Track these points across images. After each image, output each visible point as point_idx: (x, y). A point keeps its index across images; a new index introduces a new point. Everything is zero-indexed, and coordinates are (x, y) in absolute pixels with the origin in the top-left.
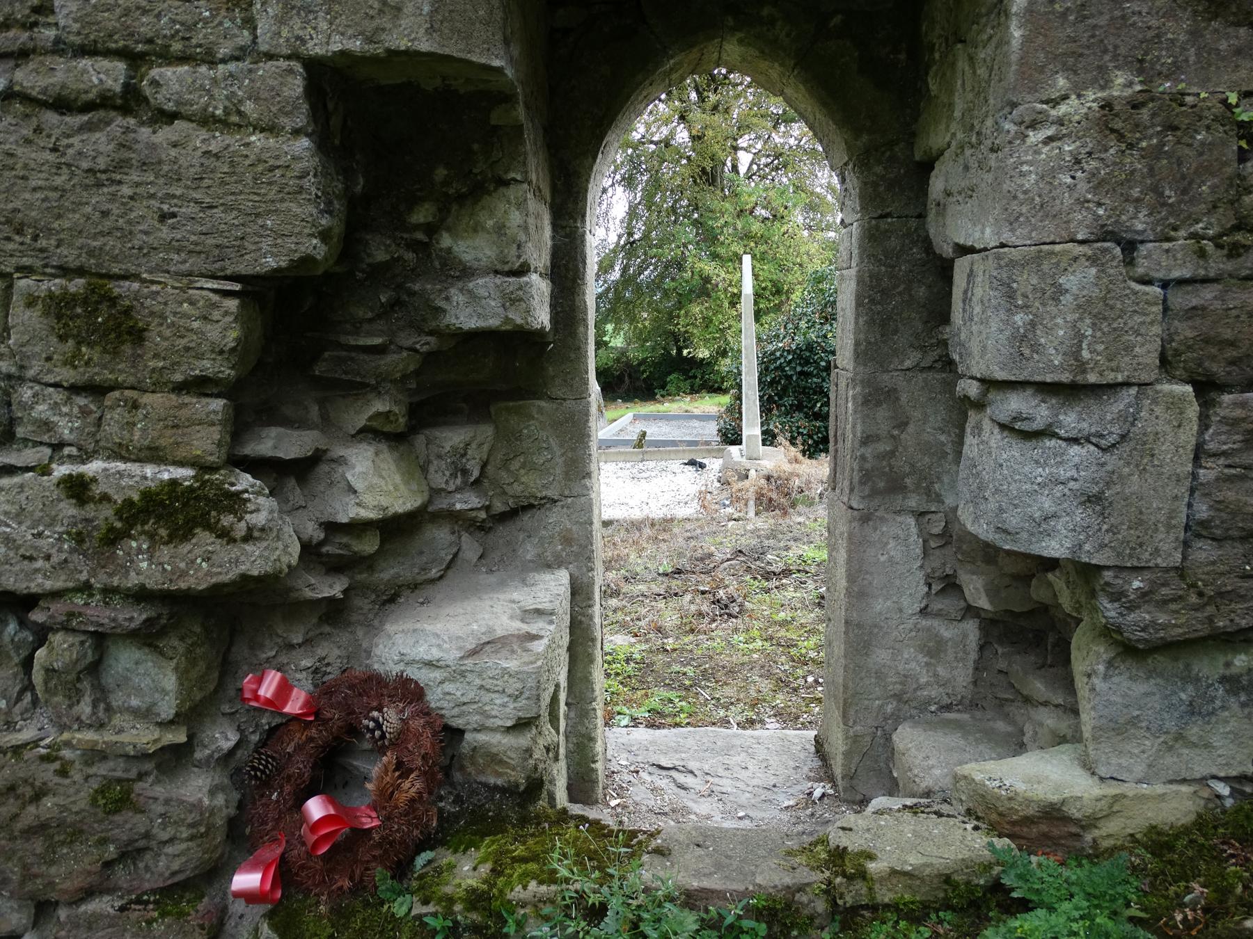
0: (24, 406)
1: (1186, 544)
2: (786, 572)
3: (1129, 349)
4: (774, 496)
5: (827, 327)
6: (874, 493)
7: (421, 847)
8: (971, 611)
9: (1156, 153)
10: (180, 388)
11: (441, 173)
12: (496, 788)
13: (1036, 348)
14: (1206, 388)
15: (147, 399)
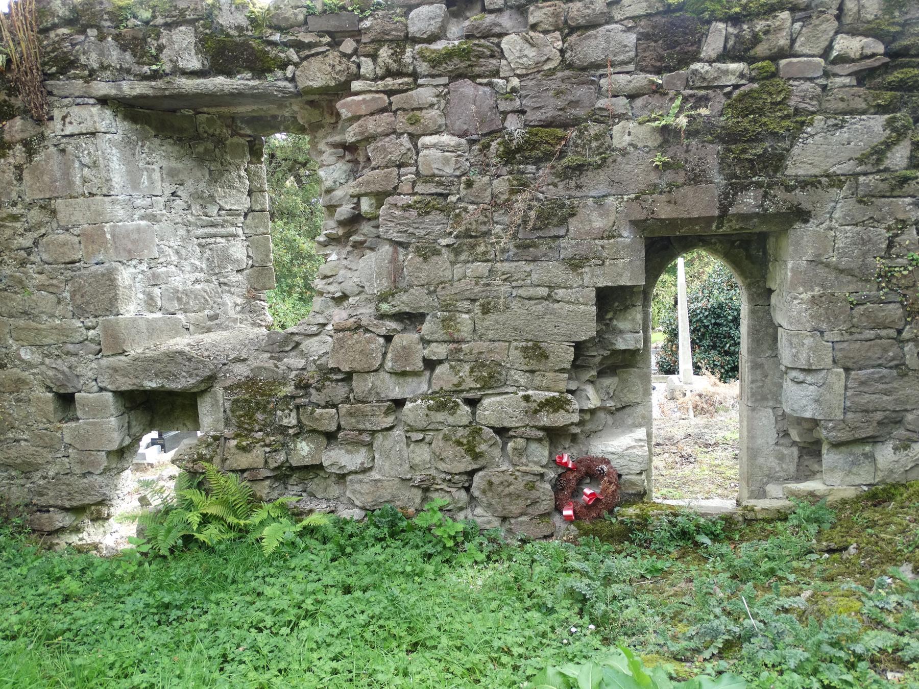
0: (511, 376)
1: (845, 413)
2: (716, 444)
3: (823, 360)
4: (705, 406)
5: (733, 292)
6: (756, 400)
7: (617, 505)
8: (794, 443)
9: (827, 309)
10: (555, 371)
11: (616, 304)
12: (632, 494)
13: (798, 359)
14: (847, 370)
15: (547, 374)
